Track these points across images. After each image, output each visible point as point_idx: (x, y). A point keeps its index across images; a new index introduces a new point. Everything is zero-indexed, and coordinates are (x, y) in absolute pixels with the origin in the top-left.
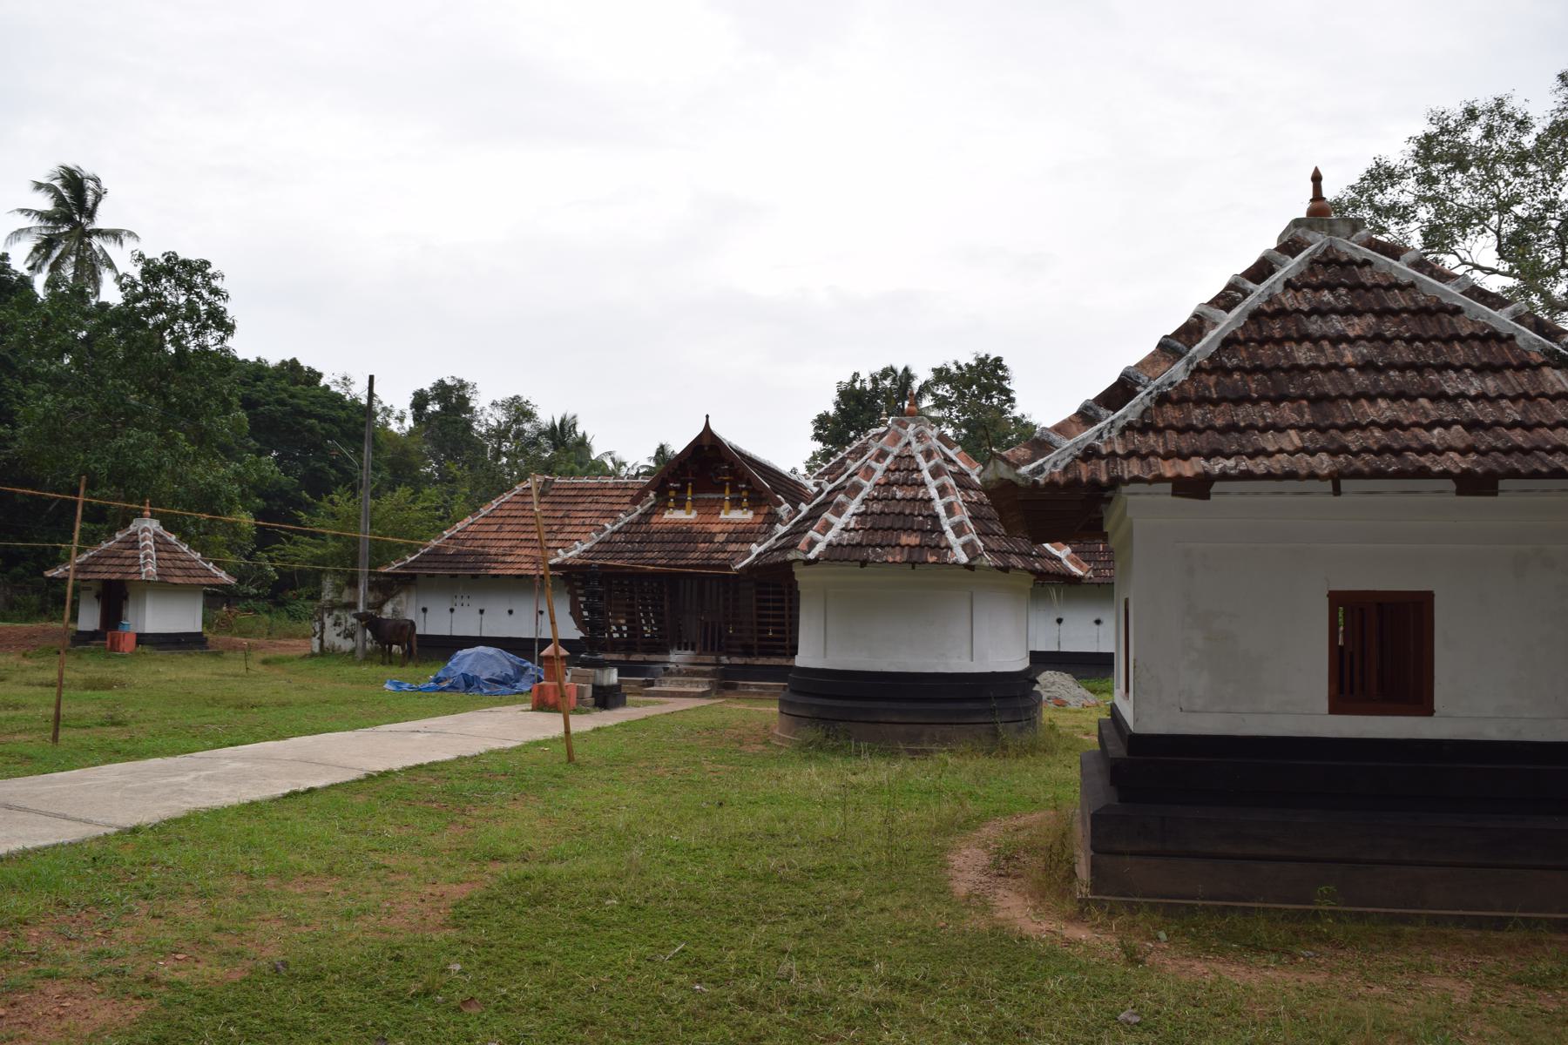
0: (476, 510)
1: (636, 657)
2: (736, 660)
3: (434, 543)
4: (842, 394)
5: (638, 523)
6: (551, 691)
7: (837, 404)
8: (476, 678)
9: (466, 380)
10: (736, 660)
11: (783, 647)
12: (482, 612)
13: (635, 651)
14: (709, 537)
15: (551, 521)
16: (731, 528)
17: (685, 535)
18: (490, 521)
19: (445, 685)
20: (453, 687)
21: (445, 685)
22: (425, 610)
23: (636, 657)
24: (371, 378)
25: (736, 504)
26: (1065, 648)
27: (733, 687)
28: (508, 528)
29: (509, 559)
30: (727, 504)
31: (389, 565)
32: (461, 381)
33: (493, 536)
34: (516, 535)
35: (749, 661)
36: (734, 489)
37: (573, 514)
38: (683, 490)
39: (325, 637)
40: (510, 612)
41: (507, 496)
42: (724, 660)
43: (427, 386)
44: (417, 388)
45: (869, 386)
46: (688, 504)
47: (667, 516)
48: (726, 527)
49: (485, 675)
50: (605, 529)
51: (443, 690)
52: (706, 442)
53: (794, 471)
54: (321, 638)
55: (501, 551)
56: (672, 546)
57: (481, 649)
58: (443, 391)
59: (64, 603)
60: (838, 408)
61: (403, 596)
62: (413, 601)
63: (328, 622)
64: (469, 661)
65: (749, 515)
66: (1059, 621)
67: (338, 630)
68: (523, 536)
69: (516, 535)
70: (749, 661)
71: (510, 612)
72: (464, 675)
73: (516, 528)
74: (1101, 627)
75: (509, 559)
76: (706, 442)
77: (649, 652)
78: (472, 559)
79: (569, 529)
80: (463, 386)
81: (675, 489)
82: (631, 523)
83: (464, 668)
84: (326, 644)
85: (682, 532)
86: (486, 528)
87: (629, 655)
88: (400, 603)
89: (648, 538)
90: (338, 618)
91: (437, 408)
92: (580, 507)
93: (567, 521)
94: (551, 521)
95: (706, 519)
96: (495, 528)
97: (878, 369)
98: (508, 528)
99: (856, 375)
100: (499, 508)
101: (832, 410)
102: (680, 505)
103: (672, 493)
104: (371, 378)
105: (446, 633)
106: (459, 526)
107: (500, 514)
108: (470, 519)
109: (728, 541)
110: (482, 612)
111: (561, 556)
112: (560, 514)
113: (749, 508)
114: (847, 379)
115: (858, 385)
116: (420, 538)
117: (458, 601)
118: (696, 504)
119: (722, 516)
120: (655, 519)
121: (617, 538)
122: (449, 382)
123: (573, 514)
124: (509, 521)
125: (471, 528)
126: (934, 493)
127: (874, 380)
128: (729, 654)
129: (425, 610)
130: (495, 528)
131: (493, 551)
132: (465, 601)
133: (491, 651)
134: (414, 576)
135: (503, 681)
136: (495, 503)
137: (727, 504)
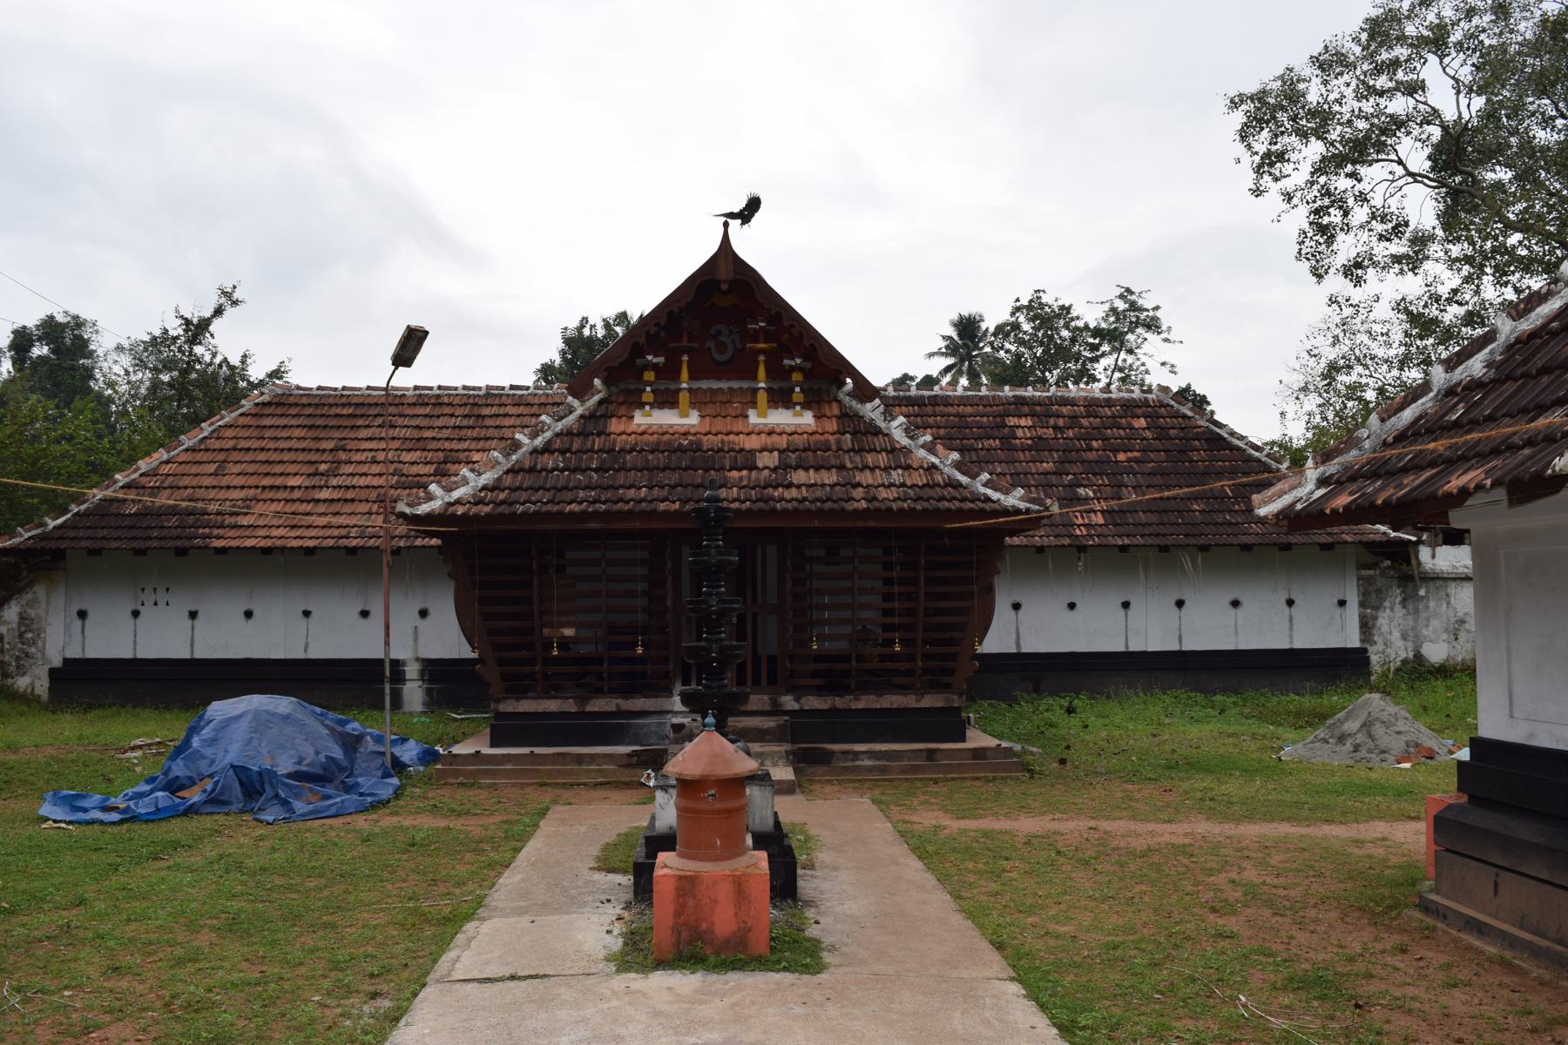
0: (174, 433)
1: (599, 705)
2: (814, 703)
3: (98, 494)
4: (568, 341)
5: (584, 434)
6: (724, 892)
7: (563, 353)
8: (267, 776)
9: (83, 316)
10: (814, 703)
11: (909, 673)
12: (193, 615)
13: (599, 692)
14: (747, 460)
15: (314, 457)
16: (782, 442)
17: (673, 449)
18: (198, 456)
19: (195, 796)
20: (216, 801)
21: (195, 796)
22: (82, 615)
23: (599, 705)
25: (780, 399)
26: (1191, 645)
27: (825, 758)
28: (236, 469)
29: (245, 521)
30: (762, 397)
31: (13, 535)
32: (76, 318)
33: (208, 481)
34: (252, 481)
35: (839, 702)
36: (776, 372)
37: (351, 445)
38: (669, 372)
40: (249, 614)
41: (228, 417)
42: (789, 702)
43: (31, 320)
44: (17, 325)
45: (601, 333)
46: (684, 398)
47: (640, 419)
48: (770, 441)
49: (285, 766)
50: (517, 445)
51: (191, 811)
52: (724, 273)
55: (227, 507)
56: (674, 478)
57: (256, 701)
58: (51, 330)
60: (564, 358)
61: (40, 591)
62: (59, 599)
64: (240, 732)
65: (807, 419)
66: (1180, 604)
68: (267, 482)
69: (252, 481)
70: (839, 702)
72: (239, 770)
73: (251, 468)
74: (1240, 611)
75: (245, 521)
76: (724, 273)
77: (629, 691)
78: (174, 521)
79: (350, 469)
80: (78, 323)
81: (655, 367)
82: (568, 433)
83: (233, 752)
85: (681, 449)
86: (194, 469)
87: (584, 700)
88: (33, 603)
89: (614, 459)
91: (45, 350)
92: (363, 433)
93: (343, 456)
94: (314, 457)
95: (719, 425)
96: (212, 468)
97: (611, 313)
98: (236, 469)
99: (584, 320)
100: (216, 434)
101: (558, 361)
102: (667, 400)
103: (649, 376)
106: (143, 465)
107: (217, 445)
108: (163, 455)
109: (784, 467)
110: (193, 615)
111: (437, 499)
112: (330, 445)
113: (806, 406)
114: (573, 323)
115: (586, 332)
116: (70, 479)
117: (149, 597)
118: (699, 401)
119: (754, 418)
120: (615, 426)
121: (549, 461)
122: (60, 318)
123: (351, 445)
124: (235, 456)
125: (166, 469)
127: (607, 325)
128: (798, 692)
129: (82, 615)
130: (212, 468)
131: (213, 507)
132: (162, 596)
133: (283, 704)
134: (59, 555)
135: (316, 777)
136: (207, 428)
137: (762, 397)
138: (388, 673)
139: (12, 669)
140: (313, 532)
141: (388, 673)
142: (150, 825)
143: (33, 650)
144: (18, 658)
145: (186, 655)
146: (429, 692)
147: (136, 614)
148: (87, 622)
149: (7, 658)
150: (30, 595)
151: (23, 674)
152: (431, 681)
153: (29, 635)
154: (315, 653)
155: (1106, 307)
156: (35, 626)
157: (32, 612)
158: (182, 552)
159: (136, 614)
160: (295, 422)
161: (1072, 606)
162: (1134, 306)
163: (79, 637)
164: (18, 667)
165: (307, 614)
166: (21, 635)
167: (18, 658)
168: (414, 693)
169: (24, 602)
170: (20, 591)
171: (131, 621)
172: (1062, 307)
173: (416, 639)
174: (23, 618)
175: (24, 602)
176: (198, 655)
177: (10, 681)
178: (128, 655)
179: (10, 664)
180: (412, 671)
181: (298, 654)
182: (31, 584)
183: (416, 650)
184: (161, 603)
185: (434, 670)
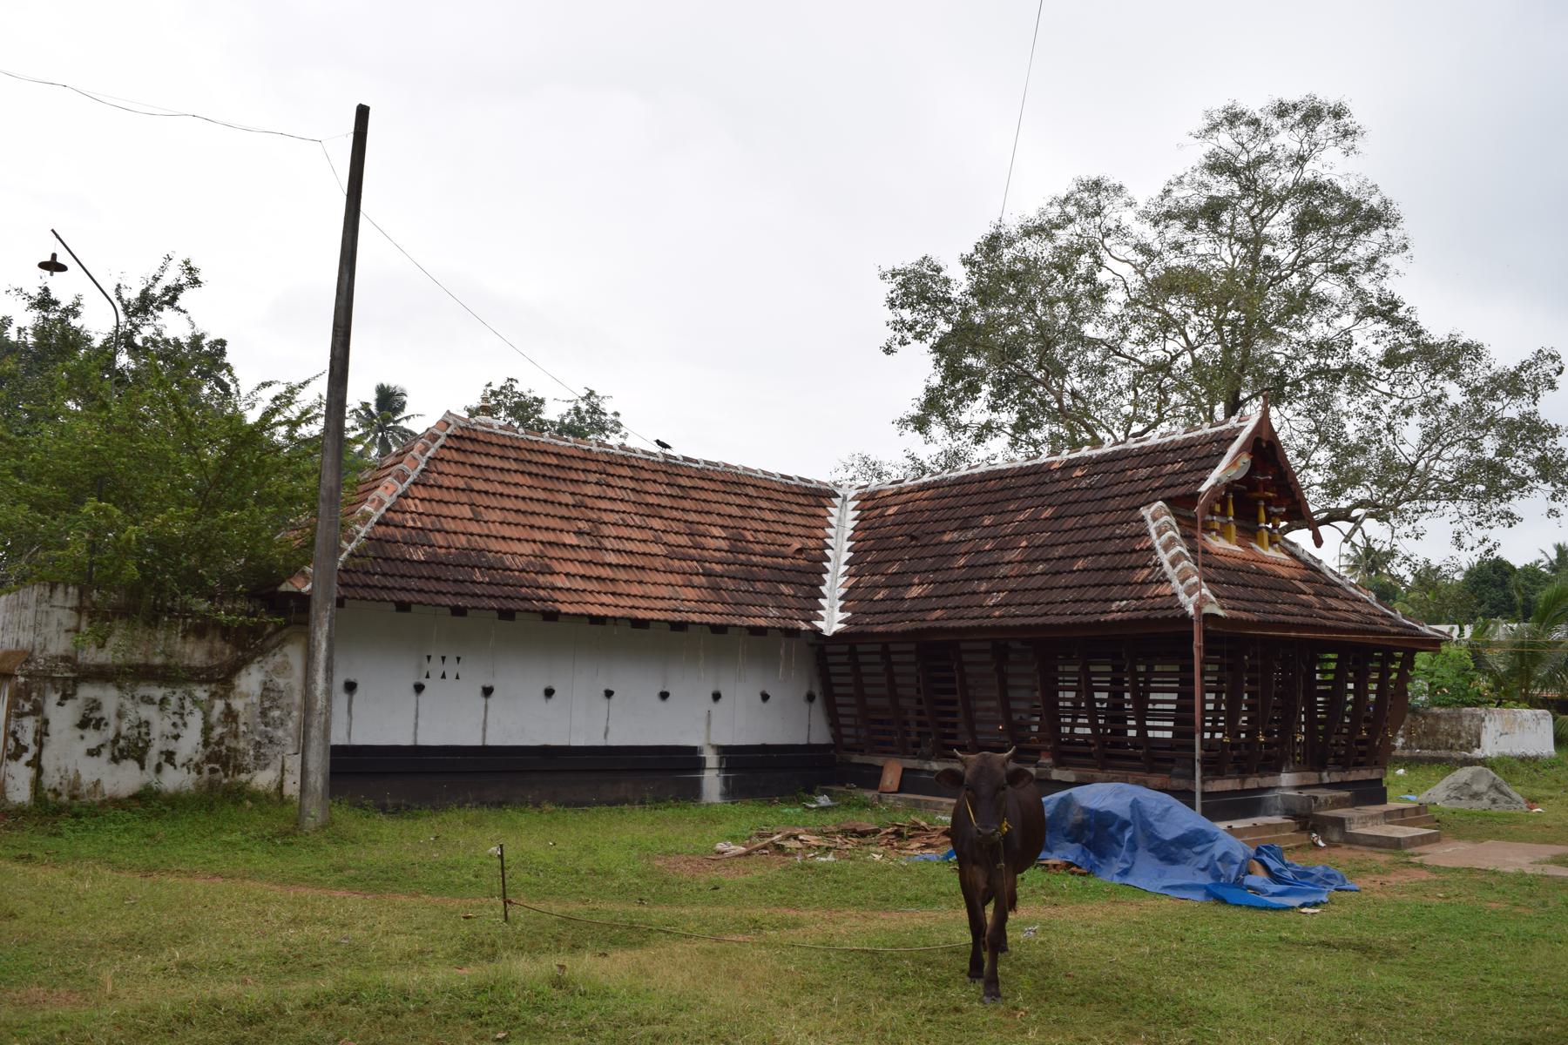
11: (1089, 755)
12: (487, 692)
24: (363, 113)
39: (46, 761)
40: (664, 696)
53: (1510, 518)
54: (36, 763)
59: (1204, 761)
63: (62, 717)
67: (93, 738)
71: (549, 693)
74: (765, 706)
84: (51, 779)
87: (1243, 780)
90: (95, 705)
104: (363, 113)
105: (406, 740)
110: (487, 692)
117: (435, 667)
126: (1176, 583)
132: (451, 667)
138: (1198, 765)
139: (249, 760)
140: (660, 604)
141: (1198, 765)
142: (1249, 913)
143: (280, 733)
144: (258, 745)
145: (477, 742)
146: (726, 781)
147: (419, 688)
148: (356, 697)
149: (242, 745)
150: (278, 658)
151: (266, 766)
152: (727, 770)
153: (276, 713)
154: (614, 740)
155: (571, 406)
156: (284, 702)
157: (281, 682)
158: (507, 615)
159: (419, 688)
160: (514, 466)
161: (664, 696)
162: (595, 410)
163: (345, 715)
164: (256, 758)
165: (609, 694)
166: (264, 713)
167: (258, 745)
168: (712, 782)
169: (269, 667)
170: (263, 652)
171: (413, 696)
172: (536, 399)
173: (709, 724)
174: (267, 689)
175: (269, 667)
176: (490, 742)
177: (243, 777)
178: (475, 740)
179: (246, 753)
180: (711, 759)
181: (598, 741)
182: (281, 644)
183: (708, 737)
184: (450, 676)
185: (733, 757)
